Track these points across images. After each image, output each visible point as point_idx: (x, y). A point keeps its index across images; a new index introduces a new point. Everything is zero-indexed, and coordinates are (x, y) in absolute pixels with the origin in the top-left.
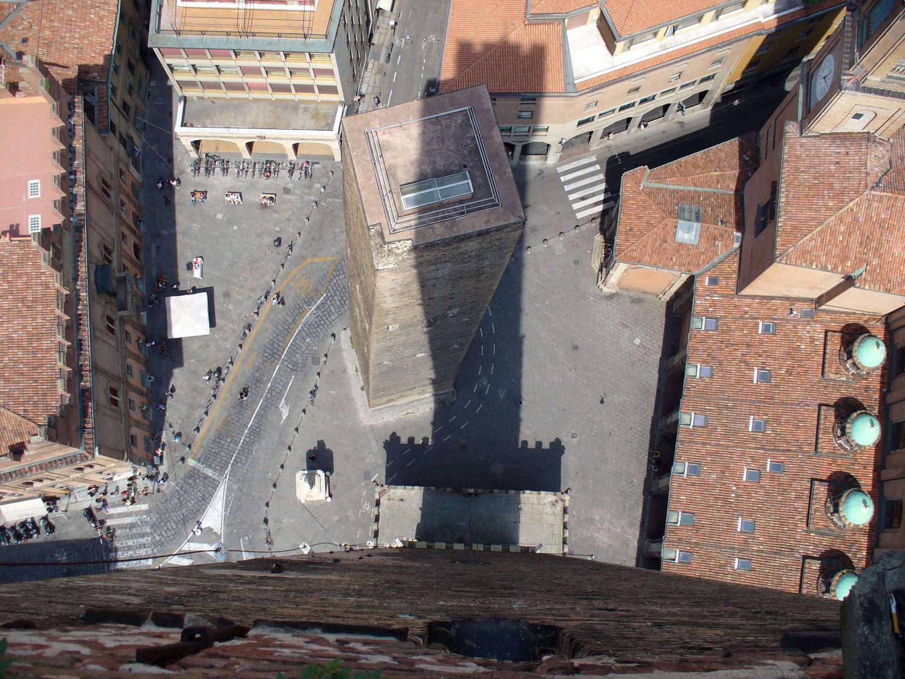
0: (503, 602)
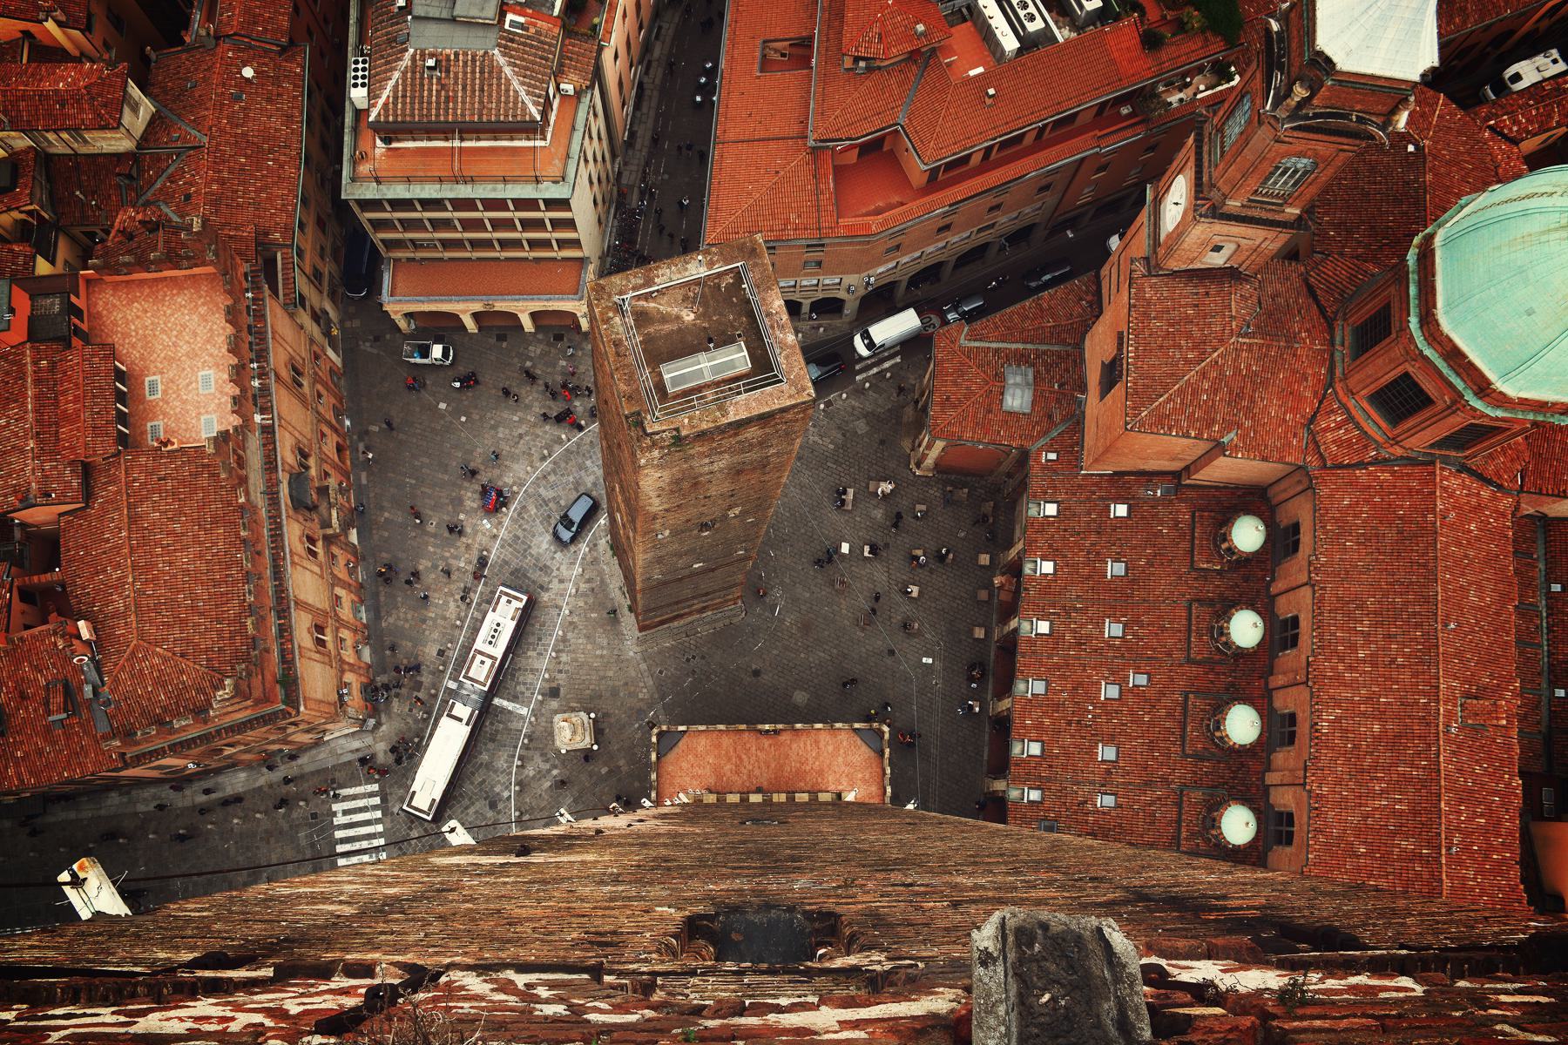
0: (783, 880)
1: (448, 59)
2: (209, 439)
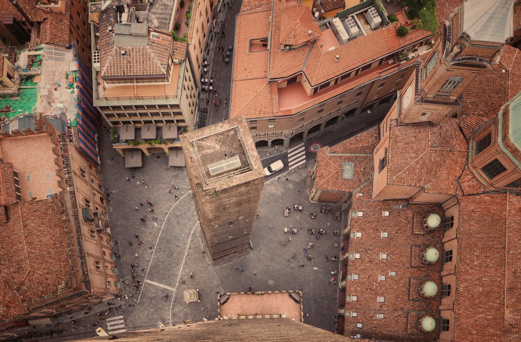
1: (130, 51)
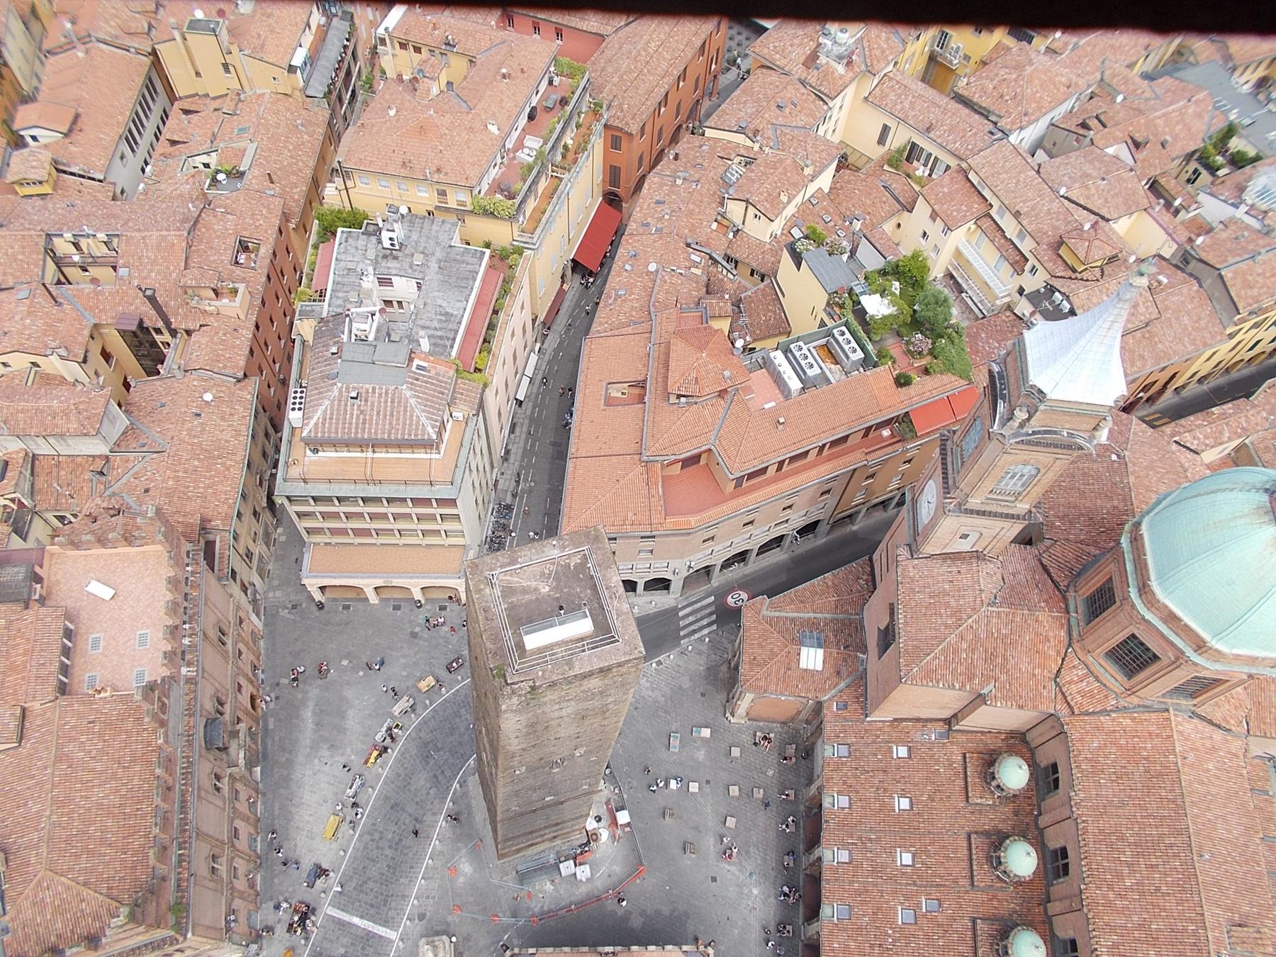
1: (367, 392)
2: (138, 687)
